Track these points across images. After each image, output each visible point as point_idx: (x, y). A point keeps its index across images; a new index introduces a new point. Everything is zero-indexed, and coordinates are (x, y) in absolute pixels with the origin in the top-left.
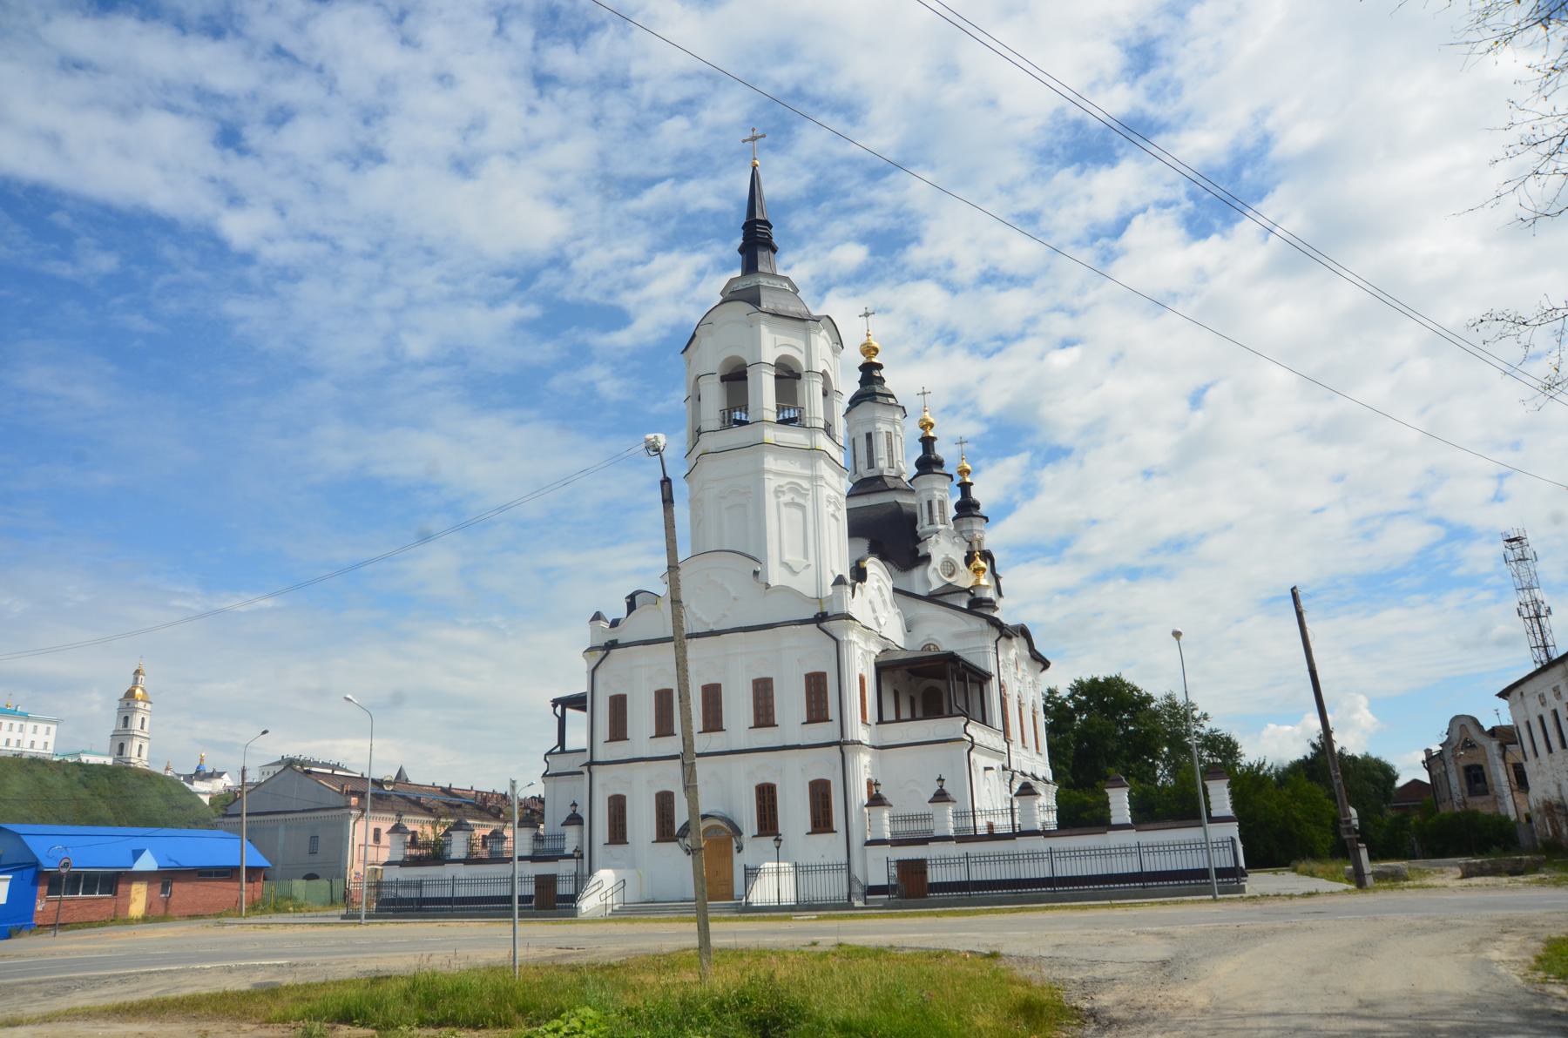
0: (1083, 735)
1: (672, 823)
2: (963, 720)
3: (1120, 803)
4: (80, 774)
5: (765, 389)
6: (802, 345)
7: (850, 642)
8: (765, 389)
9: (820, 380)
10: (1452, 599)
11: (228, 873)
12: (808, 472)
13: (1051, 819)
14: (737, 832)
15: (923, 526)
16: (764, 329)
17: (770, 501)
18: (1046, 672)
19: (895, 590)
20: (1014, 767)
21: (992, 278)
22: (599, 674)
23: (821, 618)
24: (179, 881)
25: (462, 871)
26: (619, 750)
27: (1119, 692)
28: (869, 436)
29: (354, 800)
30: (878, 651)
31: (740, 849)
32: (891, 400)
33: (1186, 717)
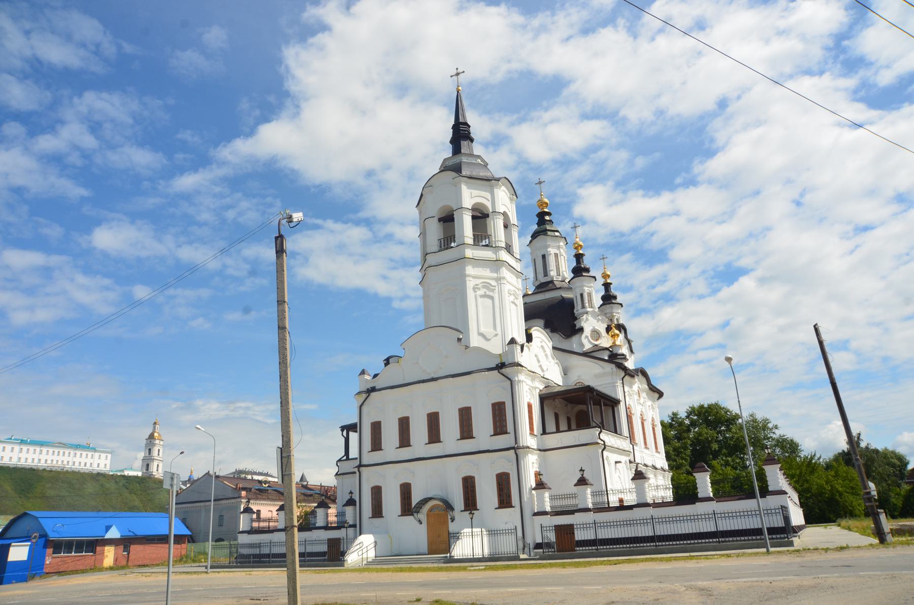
0: (697, 441)
1: (410, 504)
3: (704, 483)
4: (124, 482)
5: (466, 226)
7: (519, 381)
8: (466, 226)
9: (502, 217)
11: (163, 539)
13: (669, 495)
14: (449, 507)
15: (578, 309)
17: (470, 294)
18: (661, 400)
19: (554, 348)
20: (637, 461)
22: (364, 408)
23: (501, 366)
24: (134, 544)
26: (377, 457)
27: (717, 412)
29: (243, 493)
30: (542, 387)
31: (453, 520)
32: (557, 234)
33: (765, 427)
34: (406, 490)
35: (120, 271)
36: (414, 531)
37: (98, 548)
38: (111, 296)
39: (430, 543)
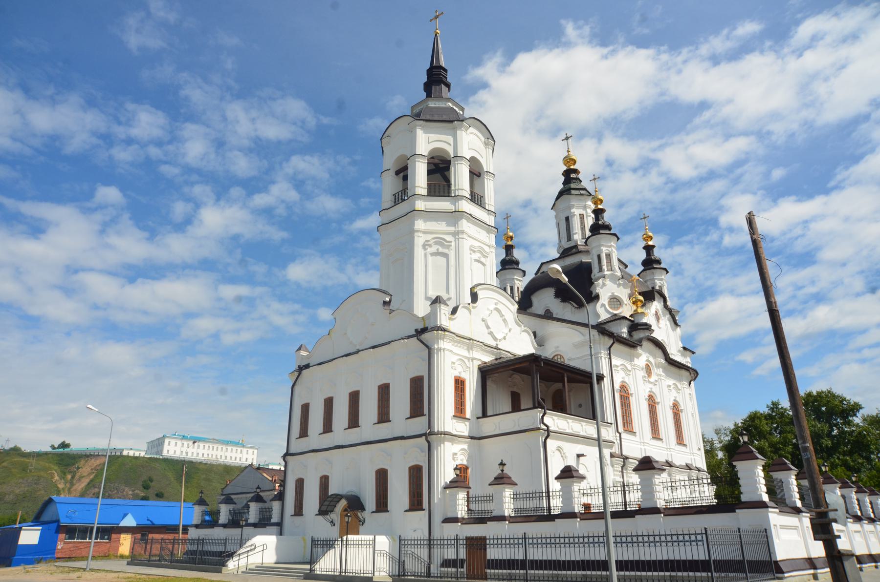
2: (539, 412)
7: (439, 349)
8: (461, 177)
17: (419, 253)
22: (296, 388)
23: (420, 332)
28: (567, 219)
32: (582, 192)
35: (306, 297)
37: (114, 536)
38: (302, 318)
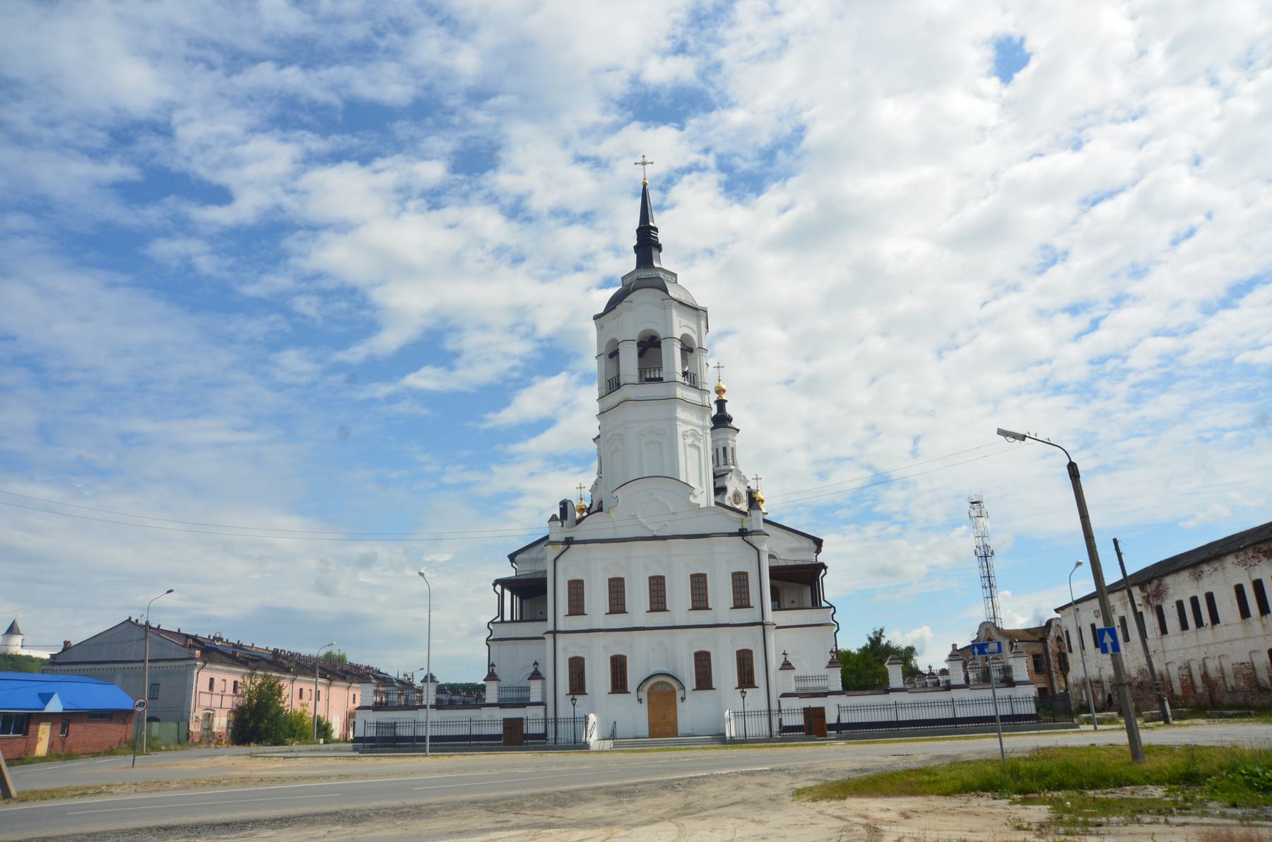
6: (694, 327)
10: (872, 529)
12: (700, 423)
16: (674, 313)
17: (680, 439)
21: (565, 216)
22: (560, 563)
23: (743, 533)
25: (435, 715)
31: (683, 699)
34: (618, 666)
36: (632, 712)
39: (652, 725)
